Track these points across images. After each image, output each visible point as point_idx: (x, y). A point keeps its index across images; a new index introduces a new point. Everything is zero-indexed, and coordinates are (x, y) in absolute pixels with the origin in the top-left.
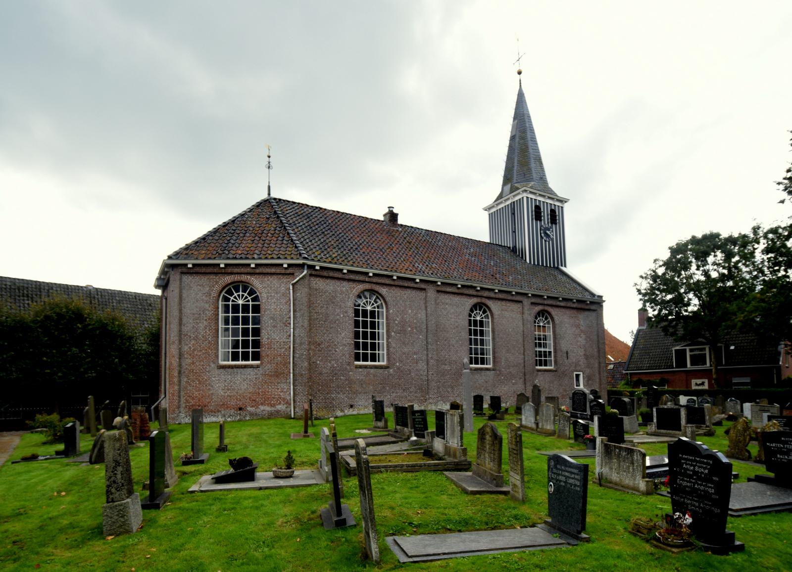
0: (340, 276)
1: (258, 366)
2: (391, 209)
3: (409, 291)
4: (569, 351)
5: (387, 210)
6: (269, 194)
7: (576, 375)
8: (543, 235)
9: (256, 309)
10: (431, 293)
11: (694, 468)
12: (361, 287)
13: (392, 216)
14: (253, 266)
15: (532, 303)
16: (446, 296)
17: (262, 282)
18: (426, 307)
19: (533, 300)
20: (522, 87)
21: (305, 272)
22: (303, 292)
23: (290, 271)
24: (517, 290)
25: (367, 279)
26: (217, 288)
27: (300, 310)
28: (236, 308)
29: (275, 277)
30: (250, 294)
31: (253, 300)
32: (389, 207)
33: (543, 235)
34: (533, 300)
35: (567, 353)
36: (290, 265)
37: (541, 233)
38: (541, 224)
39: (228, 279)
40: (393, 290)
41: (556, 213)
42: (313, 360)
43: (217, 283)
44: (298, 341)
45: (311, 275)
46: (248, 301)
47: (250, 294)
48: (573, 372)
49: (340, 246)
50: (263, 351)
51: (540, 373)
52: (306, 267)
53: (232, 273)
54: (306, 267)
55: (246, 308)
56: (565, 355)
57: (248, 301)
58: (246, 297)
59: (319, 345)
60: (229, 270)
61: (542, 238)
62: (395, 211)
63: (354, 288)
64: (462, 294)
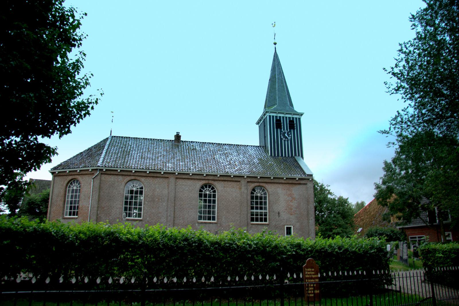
0: (117, 173)
1: (76, 218)
2: (178, 133)
3: (158, 179)
4: (280, 212)
5: (176, 134)
6: (111, 134)
7: (287, 228)
8: (282, 137)
9: (214, 196)
10: (172, 179)
11: (314, 285)
12: (129, 178)
13: (178, 137)
14: (104, 170)
15: (248, 182)
16: (183, 181)
17: (82, 178)
18: (168, 187)
19: (249, 180)
20: (277, 51)
21: (98, 172)
22: (97, 181)
23: (92, 172)
24: (261, 176)
25: (132, 174)
26: (66, 182)
27: (95, 191)
28: (205, 196)
29: (87, 176)
30: (209, 187)
31: (213, 192)
32: (177, 132)
33: (282, 137)
34: (249, 180)
35: (279, 213)
36: (92, 170)
37: (280, 137)
38: (281, 131)
39: (70, 178)
40: (148, 179)
41: (294, 122)
42: (99, 215)
43: (66, 179)
44: (92, 206)
45: (102, 174)
46: (211, 192)
47: (209, 187)
48: (284, 226)
49: (215, 154)
50: (80, 211)
51: (254, 226)
52: (98, 170)
53: (71, 175)
54: (98, 170)
55: (210, 196)
56: (277, 214)
57: (211, 192)
58: (210, 191)
59: (103, 208)
60: (71, 173)
61: (281, 139)
62: (180, 134)
63: (125, 179)
64: (192, 179)
